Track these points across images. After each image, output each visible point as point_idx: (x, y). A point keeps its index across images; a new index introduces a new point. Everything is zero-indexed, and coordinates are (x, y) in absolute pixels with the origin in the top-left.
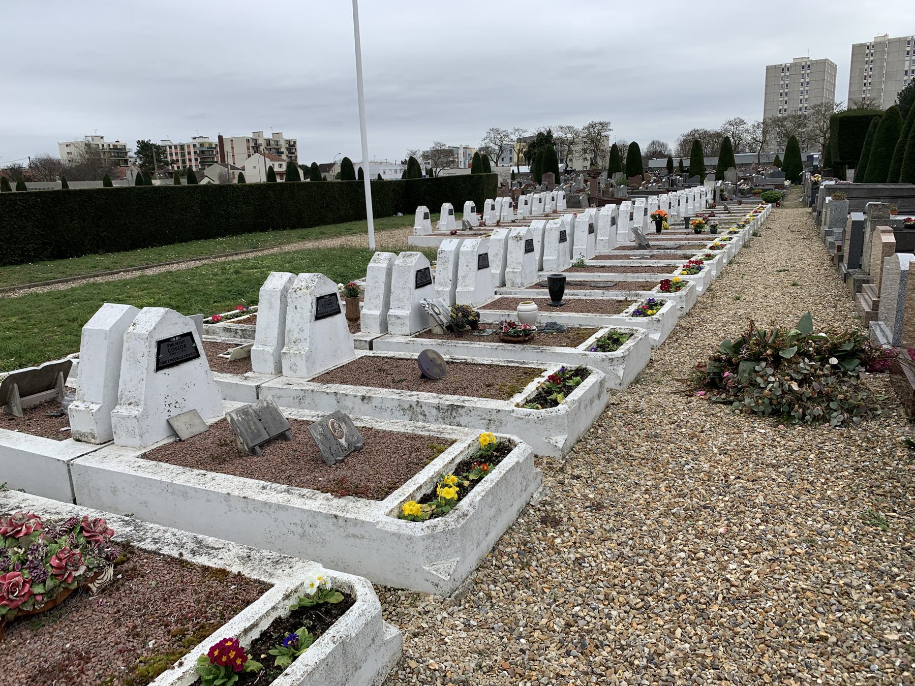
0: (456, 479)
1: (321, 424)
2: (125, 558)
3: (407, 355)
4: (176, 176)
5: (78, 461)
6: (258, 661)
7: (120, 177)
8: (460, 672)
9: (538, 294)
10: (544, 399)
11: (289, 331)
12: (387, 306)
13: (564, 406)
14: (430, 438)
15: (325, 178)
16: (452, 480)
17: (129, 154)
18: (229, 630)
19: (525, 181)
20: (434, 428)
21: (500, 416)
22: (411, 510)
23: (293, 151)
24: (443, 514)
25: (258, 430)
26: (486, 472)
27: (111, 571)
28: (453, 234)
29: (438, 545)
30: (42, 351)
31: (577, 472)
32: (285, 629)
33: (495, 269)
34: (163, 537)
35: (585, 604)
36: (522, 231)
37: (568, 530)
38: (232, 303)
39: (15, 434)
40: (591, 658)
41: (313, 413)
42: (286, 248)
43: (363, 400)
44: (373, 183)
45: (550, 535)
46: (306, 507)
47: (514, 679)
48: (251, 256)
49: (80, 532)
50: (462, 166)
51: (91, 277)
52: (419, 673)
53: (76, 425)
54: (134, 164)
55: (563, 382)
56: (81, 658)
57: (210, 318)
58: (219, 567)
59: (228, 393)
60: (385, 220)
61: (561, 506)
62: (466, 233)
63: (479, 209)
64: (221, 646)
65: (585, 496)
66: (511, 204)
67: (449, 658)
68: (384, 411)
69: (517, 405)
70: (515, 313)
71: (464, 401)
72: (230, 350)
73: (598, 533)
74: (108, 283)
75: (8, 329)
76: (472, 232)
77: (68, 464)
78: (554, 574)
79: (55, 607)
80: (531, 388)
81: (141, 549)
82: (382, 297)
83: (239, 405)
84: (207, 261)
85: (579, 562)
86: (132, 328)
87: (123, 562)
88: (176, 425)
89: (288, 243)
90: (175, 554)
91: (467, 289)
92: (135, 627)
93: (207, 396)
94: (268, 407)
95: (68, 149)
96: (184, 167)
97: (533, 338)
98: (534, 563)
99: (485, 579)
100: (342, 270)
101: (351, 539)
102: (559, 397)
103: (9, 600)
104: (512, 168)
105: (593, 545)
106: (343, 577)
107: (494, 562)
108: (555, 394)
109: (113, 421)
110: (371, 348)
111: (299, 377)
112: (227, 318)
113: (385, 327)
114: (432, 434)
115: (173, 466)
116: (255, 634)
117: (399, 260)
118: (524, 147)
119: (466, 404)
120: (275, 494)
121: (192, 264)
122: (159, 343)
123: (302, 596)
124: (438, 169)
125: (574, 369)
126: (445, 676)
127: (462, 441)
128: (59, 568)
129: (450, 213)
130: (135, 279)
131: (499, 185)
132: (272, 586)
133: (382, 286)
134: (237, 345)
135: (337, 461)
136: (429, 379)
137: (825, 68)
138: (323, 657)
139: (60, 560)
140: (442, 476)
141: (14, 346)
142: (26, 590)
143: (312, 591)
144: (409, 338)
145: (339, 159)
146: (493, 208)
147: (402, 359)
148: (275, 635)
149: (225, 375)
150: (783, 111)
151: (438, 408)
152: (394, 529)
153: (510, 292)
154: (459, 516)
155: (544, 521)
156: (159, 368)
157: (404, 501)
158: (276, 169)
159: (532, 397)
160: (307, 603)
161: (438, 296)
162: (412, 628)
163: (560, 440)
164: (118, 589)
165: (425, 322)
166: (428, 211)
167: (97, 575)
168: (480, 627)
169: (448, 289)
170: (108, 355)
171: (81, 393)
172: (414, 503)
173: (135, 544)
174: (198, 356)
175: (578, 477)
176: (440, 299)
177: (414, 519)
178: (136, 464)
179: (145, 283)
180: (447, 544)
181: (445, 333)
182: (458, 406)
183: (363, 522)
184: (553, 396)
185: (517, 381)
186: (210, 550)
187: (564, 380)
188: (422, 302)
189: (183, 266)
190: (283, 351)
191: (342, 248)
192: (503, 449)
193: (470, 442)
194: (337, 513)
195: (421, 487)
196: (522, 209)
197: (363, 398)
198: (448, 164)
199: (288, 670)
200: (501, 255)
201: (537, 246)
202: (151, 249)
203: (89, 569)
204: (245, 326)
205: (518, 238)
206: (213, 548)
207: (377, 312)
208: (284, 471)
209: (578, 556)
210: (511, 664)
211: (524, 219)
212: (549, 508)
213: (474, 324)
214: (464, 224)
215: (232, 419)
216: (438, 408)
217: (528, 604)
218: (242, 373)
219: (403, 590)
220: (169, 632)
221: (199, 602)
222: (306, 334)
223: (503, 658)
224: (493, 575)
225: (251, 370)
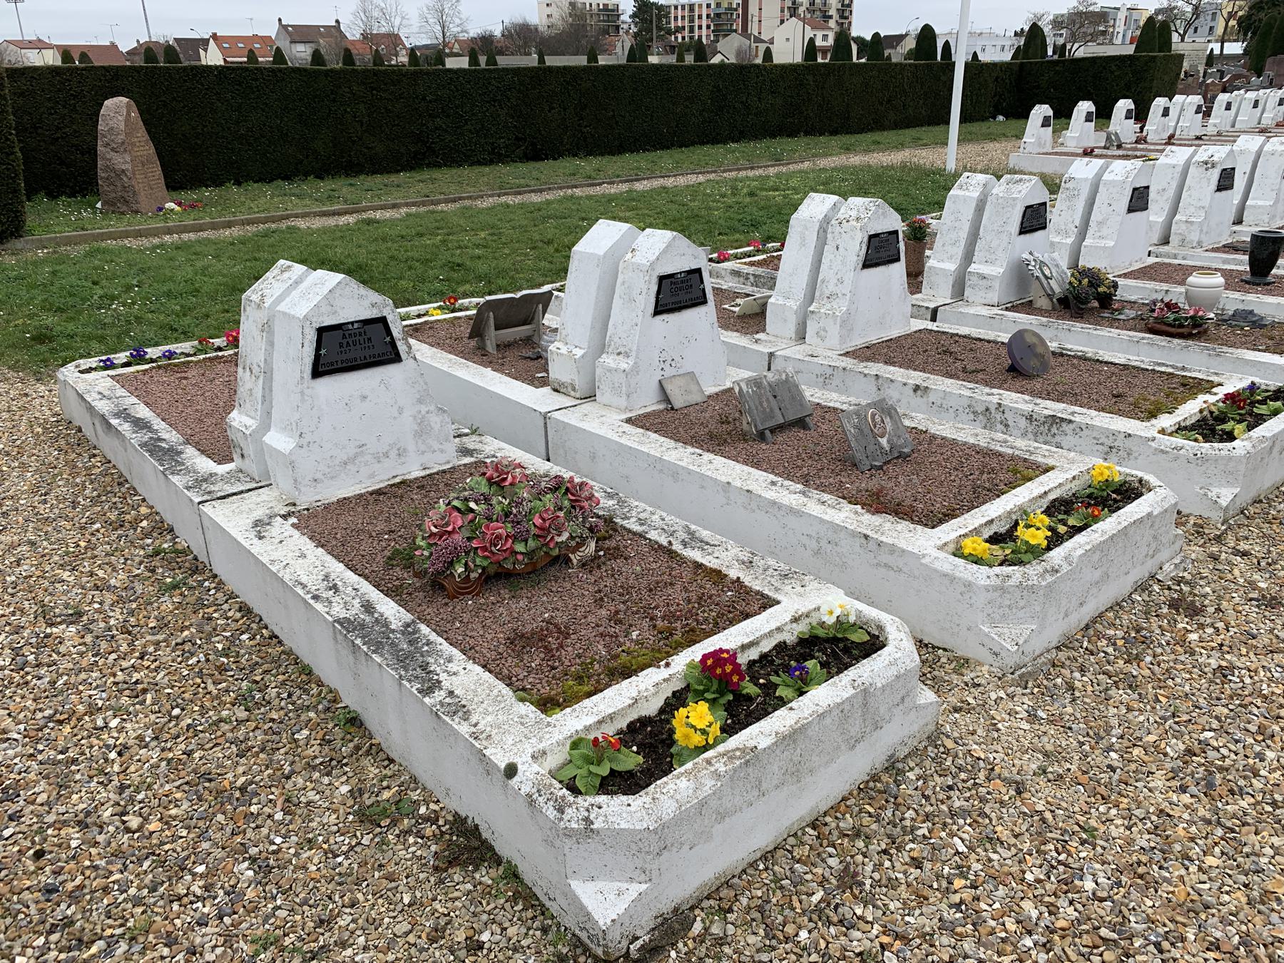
0: (1047, 520)
1: (857, 414)
2: (607, 530)
3: (990, 335)
4: (680, 50)
5: (556, 415)
6: (756, 685)
7: (608, 51)
8: (1015, 770)
9: (1225, 261)
10: (1210, 428)
11: (823, 281)
12: (968, 257)
13: (1245, 443)
14: (1012, 458)
15: (889, 58)
16: (1041, 521)
17: (622, 18)
18: (728, 639)
19: (1230, 70)
20: (1020, 445)
21: (1128, 442)
22: (975, 549)
23: (847, 14)
24: (1021, 563)
25: (772, 410)
26: (1096, 519)
27: (593, 545)
28: (1088, 153)
29: (1008, 603)
30: (512, 278)
31: (1243, 546)
32: (791, 657)
33: (1156, 214)
34: (649, 517)
35: (1222, 731)
36: (1218, 152)
37: (1212, 625)
38: (742, 237)
39: (488, 371)
40: (1220, 805)
41: (844, 398)
42: (823, 163)
43: (915, 391)
44: (967, 66)
45: (1180, 626)
46: (826, 517)
47: (1093, 800)
48: (772, 171)
49: (565, 493)
50: (1118, 40)
51: (568, 187)
52: (956, 756)
53: (557, 371)
54: (627, 32)
55: (1247, 408)
56: (559, 631)
57: (715, 255)
58: (715, 567)
59: (736, 357)
60: (975, 127)
61: (1208, 589)
62: (1109, 152)
63: (1140, 115)
64: (716, 655)
65: (1252, 585)
66: (1199, 107)
67: (1000, 749)
68: (947, 411)
69: (1162, 431)
70: (1182, 289)
71: (1073, 413)
72: (739, 301)
73: (1265, 640)
74: (589, 197)
75: (478, 246)
76: (1120, 152)
77: (545, 416)
78: (1178, 680)
79: (533, 572)
80: (1191, 409)
81: (625, 528)
82: (963, 243)
83: (747, 374)
84: (712, 176)
85: (1223, 673)
86: (630, 255)
87: (605, 539)
88: (668, 388)
89: (826, 155)
90: (663, 541)
91: (1102, 243)
92: (617, 612)
93: (708, 356)
94: (787, 380)
95: (548, 11)
96: (692, 38)
97: (1206, 331)
98: (1148, 659)
99: (1068, 663)
100: (901, 199)
101: (883, 570)
102: (1239, 429)
103: (491, 552)
104: (1211, 46)
105: (1251, 655)
106: (871, 613)
107: (1085, 644)
108: (1232, 423)
109: (598, 372)
110: (934, 319)
111: (826, 348)
112: (736, 257)
113: (959, 291)
114: (1017, 453)
115: (663, 439)
116: (754, 654)
117: (999, 188)
118: (1241, 8)
119: (1077, 418)
120: (788, 494)
121: (692, 179)
122: (321, 331)
123: (814, 624)
124: (1076, 45)
125: (1272, 388)
126: (992, 769)
127: (1062, 469)
128: (541, 529)
129: (1089, 118)
130: (621, 194)
131: (1182, 76)
132: (778, 603)
133: (966, 227)
134: (748, 295)
135: (872, 467)
136: (1021, 374)
138: (839, 701)
139: (544, 520)
140: (1025, 513)
141: (482, 267)
142: (508, 545)
143: (830, 620)
144: (996, 311)
145: (915, 28)
146: (1166, 112)
147: (980, 340)
148: (778, 661)
149: (730, 333)
151: (1030, 418)
152: (946, 568)
153: (1175, 254)
154: (1046, 571)
155: (1174, 605)
156: (657, 312)
157: (965, 536)
158: (819, 42)
159: (1188, 423)
160: (821, 633)
161: (1052, 252)
162: (954, 700)
163: (1225, 495)
164: (599, 567)
165: (1024, 290)
166: (1051, 113)
167: (579, 545)
168: (1051, 722)
169: (1069, 241)
170: (599, 287)
171: (564, 333)
172: (980, 540)
173: (618, 520)
174: (704, 302)
175: (1245, 554)
176: (1056, 255)
177: (978, 561)
178: (621, 430)
179: (633, 200)
180: (1022, 603)
181: (1054, 309)
182: (1062, 420)
183: (903, 551)
184: (1228, 426)
185: (1168, 396)
186: (703, 544)
187: (1252, 404)
188: (1026, 256)
189: (681, 181)
190: (811, 309)
191: (903, 166)
192: (1128, 492)
193: (1075, 473)
194: (869, 533)
195: (992, 521)
196: (1219, 116)
197: (917, 388)
198: (1093, 37)
199: (793, 704)
200: (1171, 193)
201: (1240, 182)
202: (642, 154)
203: (571, 538)
204: (760, 271)
205: (1208, 164)
206: (707, 544)
207: (951, 266)
208: (801, 468)
209: (1224, 664)
210: (1091, 779)
211: (1219, 134)
212: (1186, 589)
213: (1106, 301)
214: (1108, 138)
215: (741, 389)
216: (1030, 418)
217: (1129, 709)
218: (752, 333)
219: (945, 650)
220: (655, 626)
221: (689, 601)
222: (846, 287)
223: (1080, 769)
224: (1080, 660)
225: (764, 330)
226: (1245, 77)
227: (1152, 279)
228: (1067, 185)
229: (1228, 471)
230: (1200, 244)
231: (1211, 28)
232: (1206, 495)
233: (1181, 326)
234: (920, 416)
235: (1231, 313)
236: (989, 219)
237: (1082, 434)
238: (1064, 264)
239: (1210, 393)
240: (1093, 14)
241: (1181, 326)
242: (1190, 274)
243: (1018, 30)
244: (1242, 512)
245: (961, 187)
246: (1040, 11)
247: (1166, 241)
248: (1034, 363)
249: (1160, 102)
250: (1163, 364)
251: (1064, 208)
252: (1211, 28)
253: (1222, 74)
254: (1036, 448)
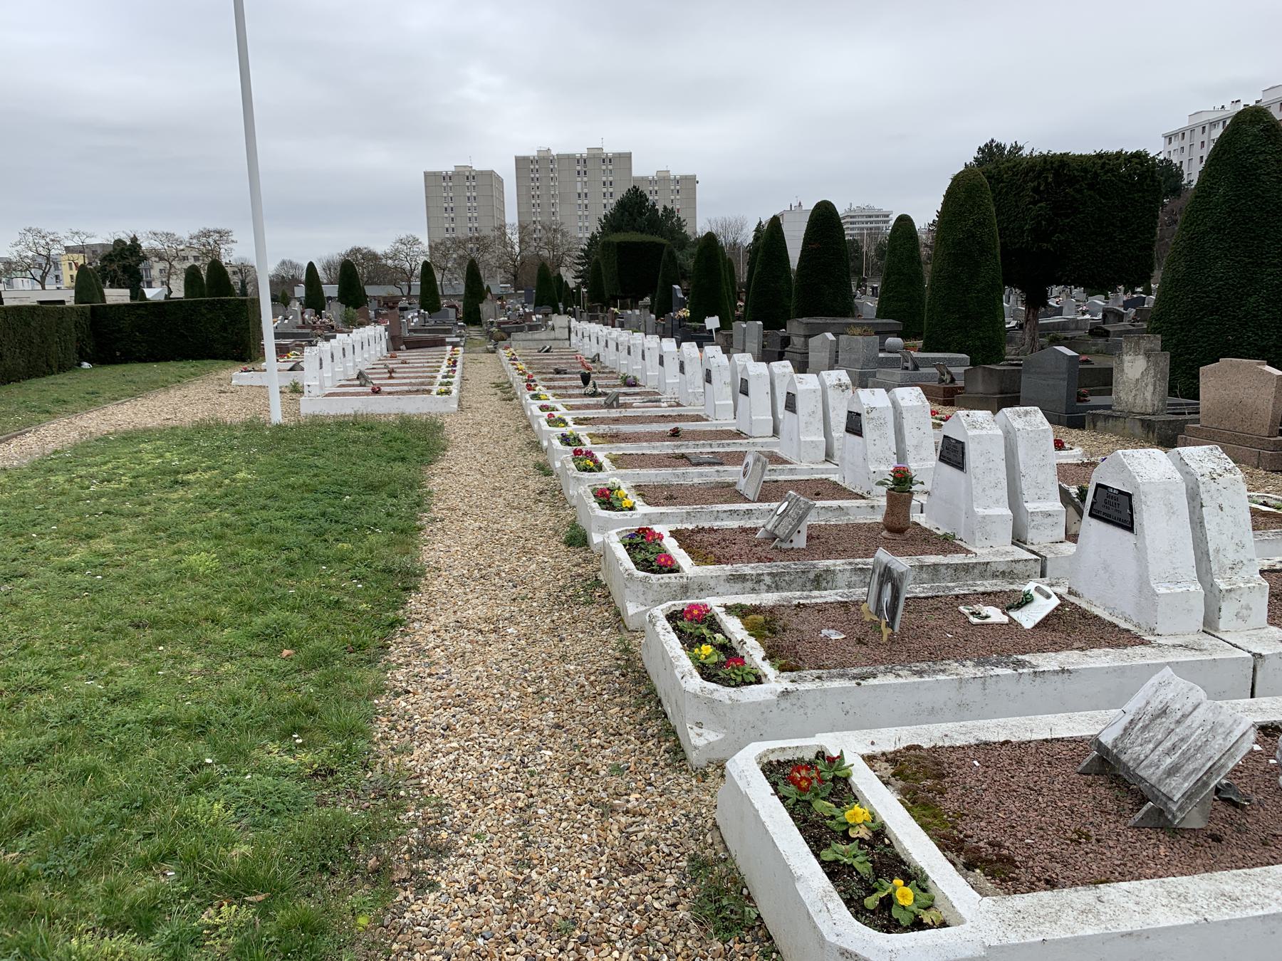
11: (1217, 551)
137: (490, 180)
228: (871, 415)
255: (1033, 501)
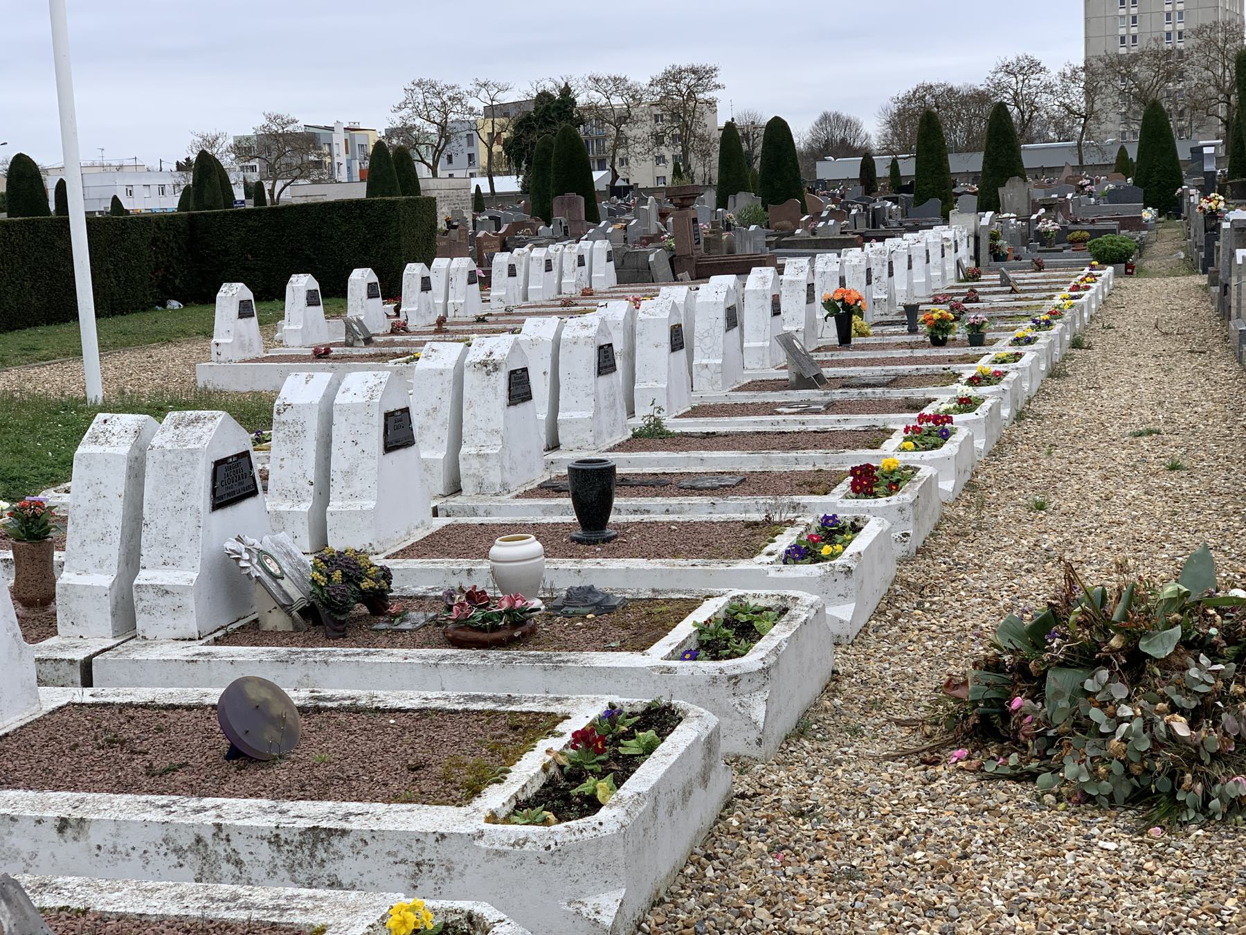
3: (190, 695)
9: (546, 511)
10: (563, 796)
12: (131, 560)
19: (510, 215)
28: (322, 354)
33: (430, 447)
36: (499, 346)
55: (612, 747)
60: (131, 322)
62: (354, 351)
63: (389, 289)
66: (472, 274)
69: (493, 818)
70: (486, 565)
71: (346, 817)
80: (528, 769)
82: (117, 535)
91: (356, 505)
97: (533, 631)
102: (602, 787)
104: (474, 182)
108: (591, 780)
110: (87, 682)
113: (126, 619)
114: (256, 915)
117: (165, 434)
118: (503, 128)
119: (355, 824)
124: (279, 184)
125: (640, 709)
129: (312, 300)
144: (197, 647)
146: (426, 285)
147: (173, 707)
150: (1129, 40)
151: (275, 840)
153: (475, 508)
159: (530, 793)
161: (276, 530)
166: (249, 295)
169: (305, 507)
181: (297, 629)
182: (330, 832)
184: (585, 788)
187: (616, 741)
188: (231, 545)
198: (304, 171)
200: (446, 412)
201: (539, 386)
205: (488, 366)
207: (104, 580)
211: (508, 312)
213: (378, 601)
214: (349, 329)
226: (530, 225)
227: (446, 554)
228: (283, 417)
229: (602, 862)
230: (505, 487)
231: (471, 156)
232: (578, 913)
233: (495, 628)
234: (74, 881)
235: (564, 594)
236: (156, 489)
237: (366, 850)
238: (306, 543)
239: (552, 734)
240: (294, 136)
241: (495, 628)
242: (491, 542)
243: (182, 160)
244: (639, 928)
245: (95, 440)
246: (211, 132)
247: (456, 489)
248: (270, 735)
249: (413, 272)
250: (679, 591)
251: (284, 454)
252: (471, 156)
253: (497, 222)
254: (290, 898)
255: (154, 567)
